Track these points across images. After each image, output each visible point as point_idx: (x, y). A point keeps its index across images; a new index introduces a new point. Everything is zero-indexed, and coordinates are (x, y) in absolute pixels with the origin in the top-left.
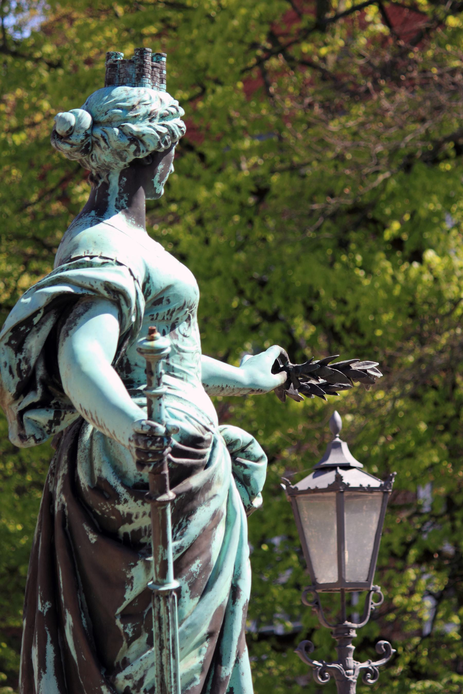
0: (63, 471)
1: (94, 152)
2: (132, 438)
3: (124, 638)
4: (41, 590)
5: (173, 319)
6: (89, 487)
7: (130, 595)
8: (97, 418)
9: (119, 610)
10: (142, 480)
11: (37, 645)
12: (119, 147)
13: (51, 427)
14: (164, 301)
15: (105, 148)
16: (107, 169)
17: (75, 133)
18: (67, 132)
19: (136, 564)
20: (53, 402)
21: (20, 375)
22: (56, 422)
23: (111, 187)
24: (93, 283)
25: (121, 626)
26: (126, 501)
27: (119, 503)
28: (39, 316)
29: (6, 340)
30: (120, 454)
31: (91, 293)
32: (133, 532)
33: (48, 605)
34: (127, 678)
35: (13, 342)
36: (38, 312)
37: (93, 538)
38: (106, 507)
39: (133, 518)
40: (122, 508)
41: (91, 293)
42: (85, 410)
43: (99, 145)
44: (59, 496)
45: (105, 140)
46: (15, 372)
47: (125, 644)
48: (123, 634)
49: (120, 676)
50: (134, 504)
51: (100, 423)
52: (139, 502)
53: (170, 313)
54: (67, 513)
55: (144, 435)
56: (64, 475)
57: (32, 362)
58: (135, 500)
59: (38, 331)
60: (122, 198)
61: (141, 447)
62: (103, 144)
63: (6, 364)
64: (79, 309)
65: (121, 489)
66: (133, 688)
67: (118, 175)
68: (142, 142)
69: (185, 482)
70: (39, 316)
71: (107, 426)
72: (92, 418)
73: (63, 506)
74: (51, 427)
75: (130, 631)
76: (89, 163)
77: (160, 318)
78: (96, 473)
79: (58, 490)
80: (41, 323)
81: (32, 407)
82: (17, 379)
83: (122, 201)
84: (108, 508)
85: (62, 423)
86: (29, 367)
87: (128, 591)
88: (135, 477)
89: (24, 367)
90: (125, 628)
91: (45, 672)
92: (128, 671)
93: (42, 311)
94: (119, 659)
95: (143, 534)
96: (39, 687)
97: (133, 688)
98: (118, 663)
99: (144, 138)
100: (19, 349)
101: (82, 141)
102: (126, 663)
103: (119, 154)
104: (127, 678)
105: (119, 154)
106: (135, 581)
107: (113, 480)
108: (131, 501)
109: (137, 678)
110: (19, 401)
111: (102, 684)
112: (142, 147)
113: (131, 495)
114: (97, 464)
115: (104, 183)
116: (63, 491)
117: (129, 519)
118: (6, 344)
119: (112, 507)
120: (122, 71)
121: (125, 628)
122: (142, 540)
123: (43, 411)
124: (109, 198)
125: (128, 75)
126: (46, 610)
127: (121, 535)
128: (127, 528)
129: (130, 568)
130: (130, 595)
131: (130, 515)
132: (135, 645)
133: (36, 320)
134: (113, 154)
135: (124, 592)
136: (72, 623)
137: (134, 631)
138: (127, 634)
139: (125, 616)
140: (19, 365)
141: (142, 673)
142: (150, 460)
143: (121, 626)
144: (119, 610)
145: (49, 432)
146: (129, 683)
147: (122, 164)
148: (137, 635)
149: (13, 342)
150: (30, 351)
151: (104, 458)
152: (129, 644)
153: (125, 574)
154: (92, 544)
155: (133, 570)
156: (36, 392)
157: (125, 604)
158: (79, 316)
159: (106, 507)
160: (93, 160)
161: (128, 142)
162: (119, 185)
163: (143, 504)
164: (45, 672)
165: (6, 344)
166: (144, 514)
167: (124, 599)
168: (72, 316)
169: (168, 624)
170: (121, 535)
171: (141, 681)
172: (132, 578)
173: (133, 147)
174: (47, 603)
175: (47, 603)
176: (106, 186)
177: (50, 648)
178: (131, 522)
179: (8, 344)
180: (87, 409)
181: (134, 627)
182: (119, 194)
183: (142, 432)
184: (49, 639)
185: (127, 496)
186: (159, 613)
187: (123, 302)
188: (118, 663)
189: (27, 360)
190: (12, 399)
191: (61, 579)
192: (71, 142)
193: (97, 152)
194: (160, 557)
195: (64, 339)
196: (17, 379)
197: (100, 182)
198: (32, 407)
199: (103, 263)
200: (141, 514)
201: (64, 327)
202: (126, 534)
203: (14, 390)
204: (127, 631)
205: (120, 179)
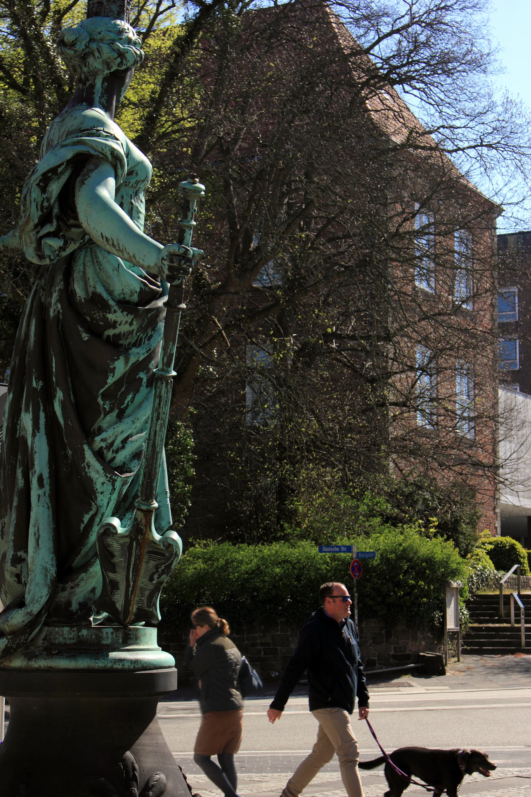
0: (59, 286)
1: (88, 60)
2: (165, 258)
3: (102, 412)
4: (35, 372)
5: (137, 188)
6: (85, 299)
7: (111, 381)
8: (118, 244)
9: (101, 391)
10: (125, 298)
11: (31, 413)
12: (109, 58)
13: (59, 252)
14: (134, 174)
15: (98, 57)
16: (94, 74)
17: (78, 43)
18: (73, 41)
19: (119, 358)
20: (61, 234)
21: (42, 210)
22: (62, 249)
23: (96, 88)
24: (104, 148)
25: (102, 403)
26: (115, 312)
27: (109, 313)
28: (63, 167)
29: (37, 182)
30: (109, 278)
31: (101, 156)
32: (114, 335)
33: (41, 383)
34: (102, 440)
35: (41, 184)
36: (62, 164)
37: (85, 337)
38: (97, 315)
39: (117, 325)
40: (111, 317)
41: (101, 156)
42: (106, 238)
43: (94, 55)
44: (56, 304)
45: (99, 52)
46: (39, 207)
47: (102, 415)
48: (101, 409)
49: (98, 439)
50: (121, 314)
51: (121, 248)
52: (125, 313)
53: (137, 182)
54: (61, 317)
55: (179, 256)
56: (60, 289)
57: (52, 201)
58: (122, 312)
59: (58, 178)
60: (103, 97)
61: (175, 265)
62: (97, 54)
63: (35, 199)
64: (91, 167)
65: (111, 303)
66: (105, 449)
67: (101, 80)
68: (125, 57)
69: (153, 302)
70: (63, 167)
71: (127, 250)
72: (113, 244)
73: (59, 312)
74: (59, 252)
75: (107, 407)
76: (81, 68)
77: (130, 185)
78: (91, 290)
79: (53, 301)
80: (62, 173)
81: (48, 235)
82: (40, 213)
83: (103, 99)
84: (99, 316)
85: (67, 250)
86: (50, 205)
87: (110, 378)
88: (119, 295)
89: (46, 204)
90: (104, 404)
91: (39, 432)
92: (103, 435)
93: (65, 164)
94: (96, 426)
95: (122, 337)
96: (33, 443)
97: (105, 449)
98: (94, 429)
99: (127, 55)
100: (44, 190)
101: (83, 50)
102: (100, 430)
103: (107, 64)
104: (102, 440)
105: (107, 64)
106: (116, 371)
107: (105, 295)
108: (119, 312)
109: (109, 441)
110: (37, 230)
111: (85, 444)
112: (124, 62)
113: (120, 308)
114: (91, 282)
115: (91, 84)
116: (59, 300)
117: (114, 325)
118: (37, 185)
119: (103, 315)
120: (107, 7)
121: (104, 404)
122: (121, 342)
123: (56, 239)
124: (95, 95)
125: (111, 11)
126: (39, 387)
127: (105, 336)
128: (111, 332)
129: (114, 361)
130: (111, 381)
131: (115, 322)
132: (108, 418)
133: (60, 170)
134: (103, 64)
135: (107, 378)
136: (62, 398)
137: (110, 407)
138: (105, 409)
139: (105, 396)
140: (42, 202)
141: (114, 438)
142: (181, 275)
143: (102, 403)
144: (101, 391)
145: (58, 255)
146: (103, 445)
147: (107, 72)
148: (111, 410)
149: (41, 184)
150: (51, 193)
151: (96, 279)
152: (105, 416)
153: (109, 365)
154: (84, 341)
155: (116, 362)
156: (52, 225)
157: (106, 387)
158: (92, 171)
159: (97, 315)
160: (85, 66)
161: (116, 55)
162: (102, 87)
163: (127, 315)
164: (39, 432)
165: (37, 185)
166: (126, 322)
167: (107, 383)
168: (85, 171)
169: (166, 402)
170: (105, 336)
171: (112, 443)
172: (115, 368)
173: (119, 60)
174: (40, 382)
175: (40, 382)
176: (92, 86)
177: (42, 415)
178: (115, 327)
179: (38, 185)
180: (109, 237)
181: (110, 404)
182: (101, 93)
183: (179, 253)
184: (42, 408)
185: (116, 308)
186: (160, 393)
187: (119, 166)
188: (94, 429)
189: (48, 200)
190: (33, 227)
191: (54, 365)
192: (75, 49)
193: (91, 60)
194: (169, 351)
195: (81, 187)
196: (40, 213)
197: (88, 84)
198: (48, 235)
199: (107, 136)
200: (124, 322)
201: (79, 178)
202: (108, 336)
203: (36, 221)
204: (105, 406)
205: (103, 83)
